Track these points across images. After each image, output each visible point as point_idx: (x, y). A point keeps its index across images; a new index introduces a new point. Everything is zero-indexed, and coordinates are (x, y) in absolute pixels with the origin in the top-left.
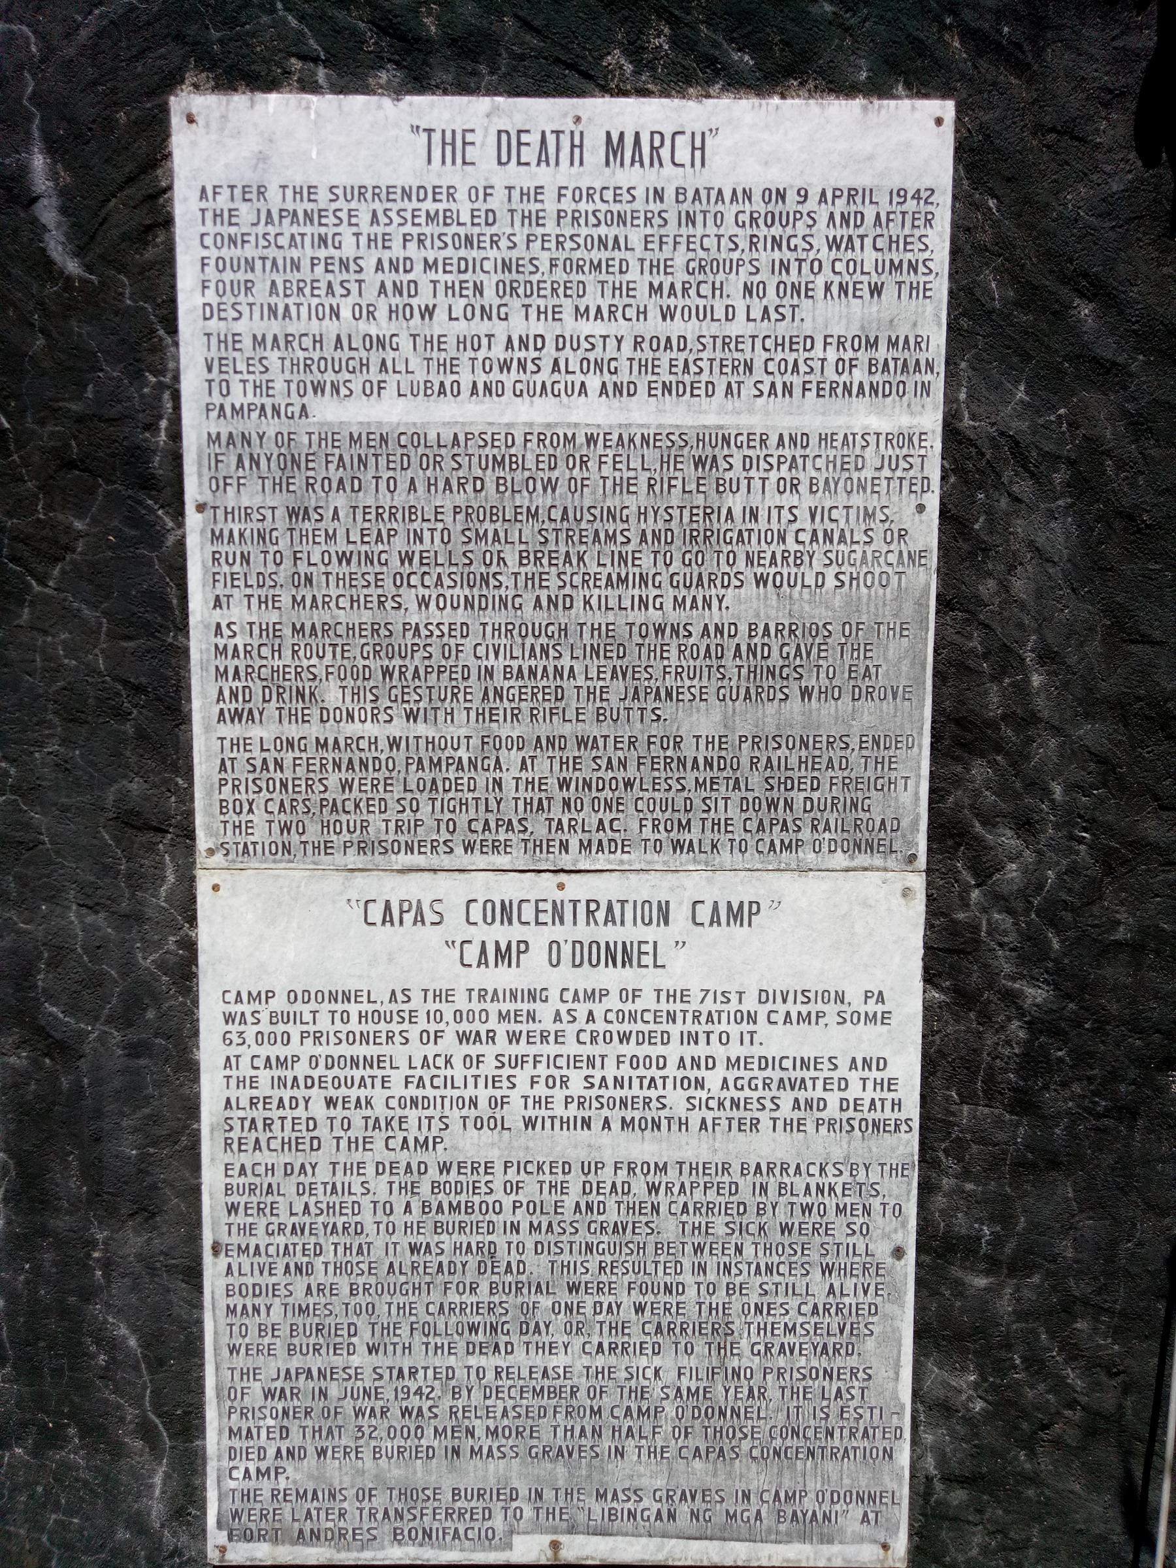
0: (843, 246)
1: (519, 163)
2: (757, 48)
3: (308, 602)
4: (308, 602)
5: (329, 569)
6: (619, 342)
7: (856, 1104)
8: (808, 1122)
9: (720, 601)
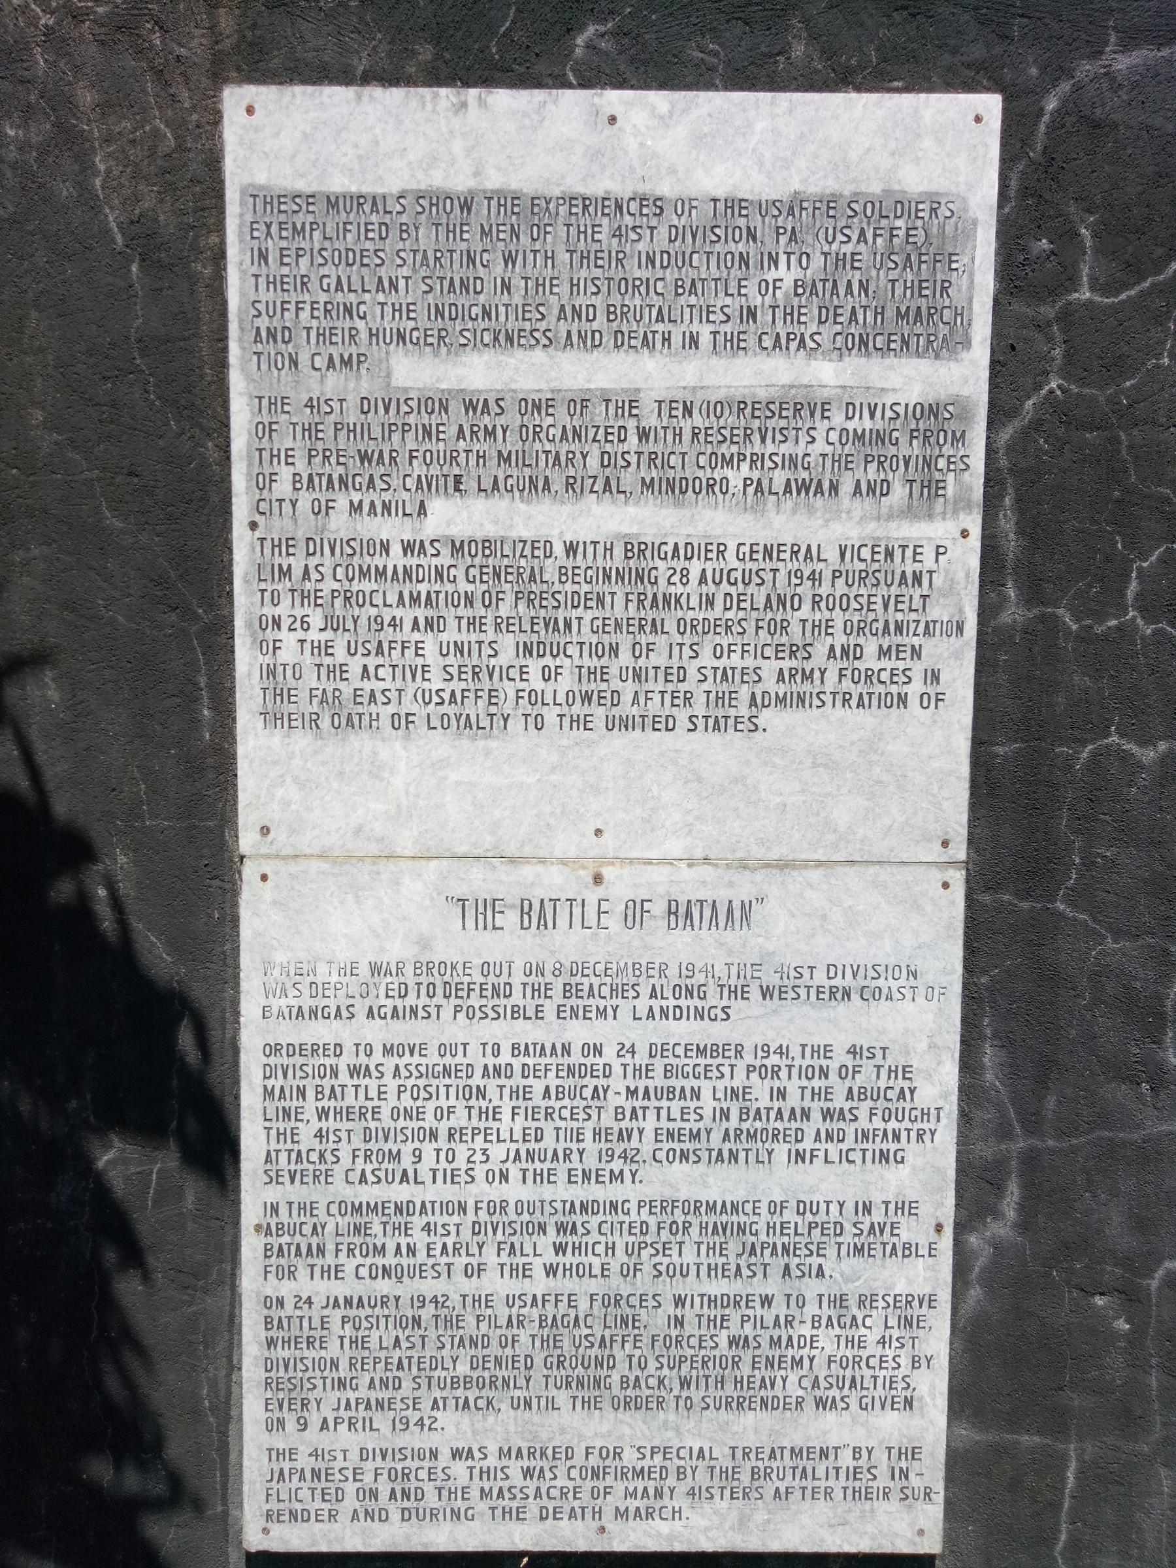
0: (813, 489)
1: (371, 1429)
2: (1011, 448)
3: (366, 508)
4: (366, 508)
5: (471, 1103)
6: (841, 1206)
7: (555, 1513)
8: (418, 308)
9: (633, 1176)
